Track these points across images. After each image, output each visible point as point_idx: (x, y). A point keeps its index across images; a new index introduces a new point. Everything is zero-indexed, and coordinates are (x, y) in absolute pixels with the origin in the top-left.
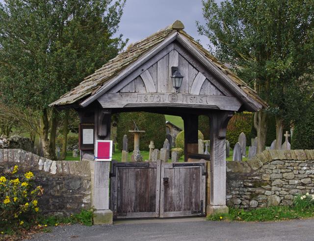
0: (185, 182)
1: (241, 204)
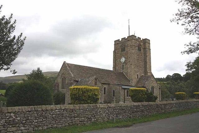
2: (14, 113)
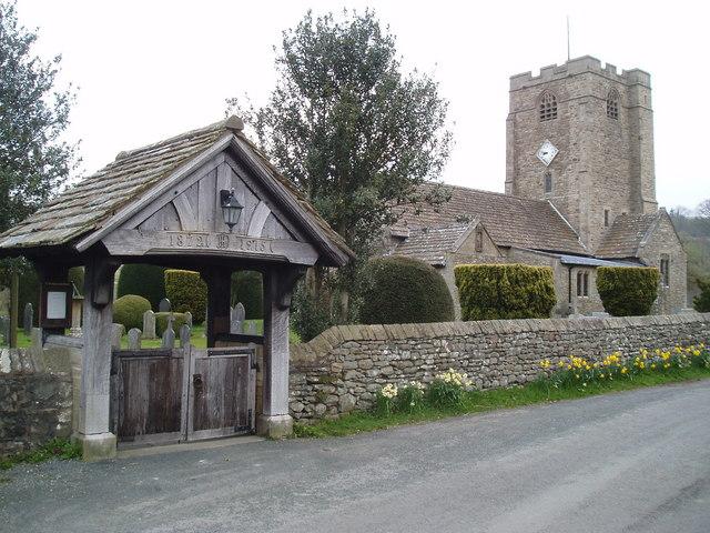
0: (226, 381)
1: (304, 411)
2: (447, 338)
